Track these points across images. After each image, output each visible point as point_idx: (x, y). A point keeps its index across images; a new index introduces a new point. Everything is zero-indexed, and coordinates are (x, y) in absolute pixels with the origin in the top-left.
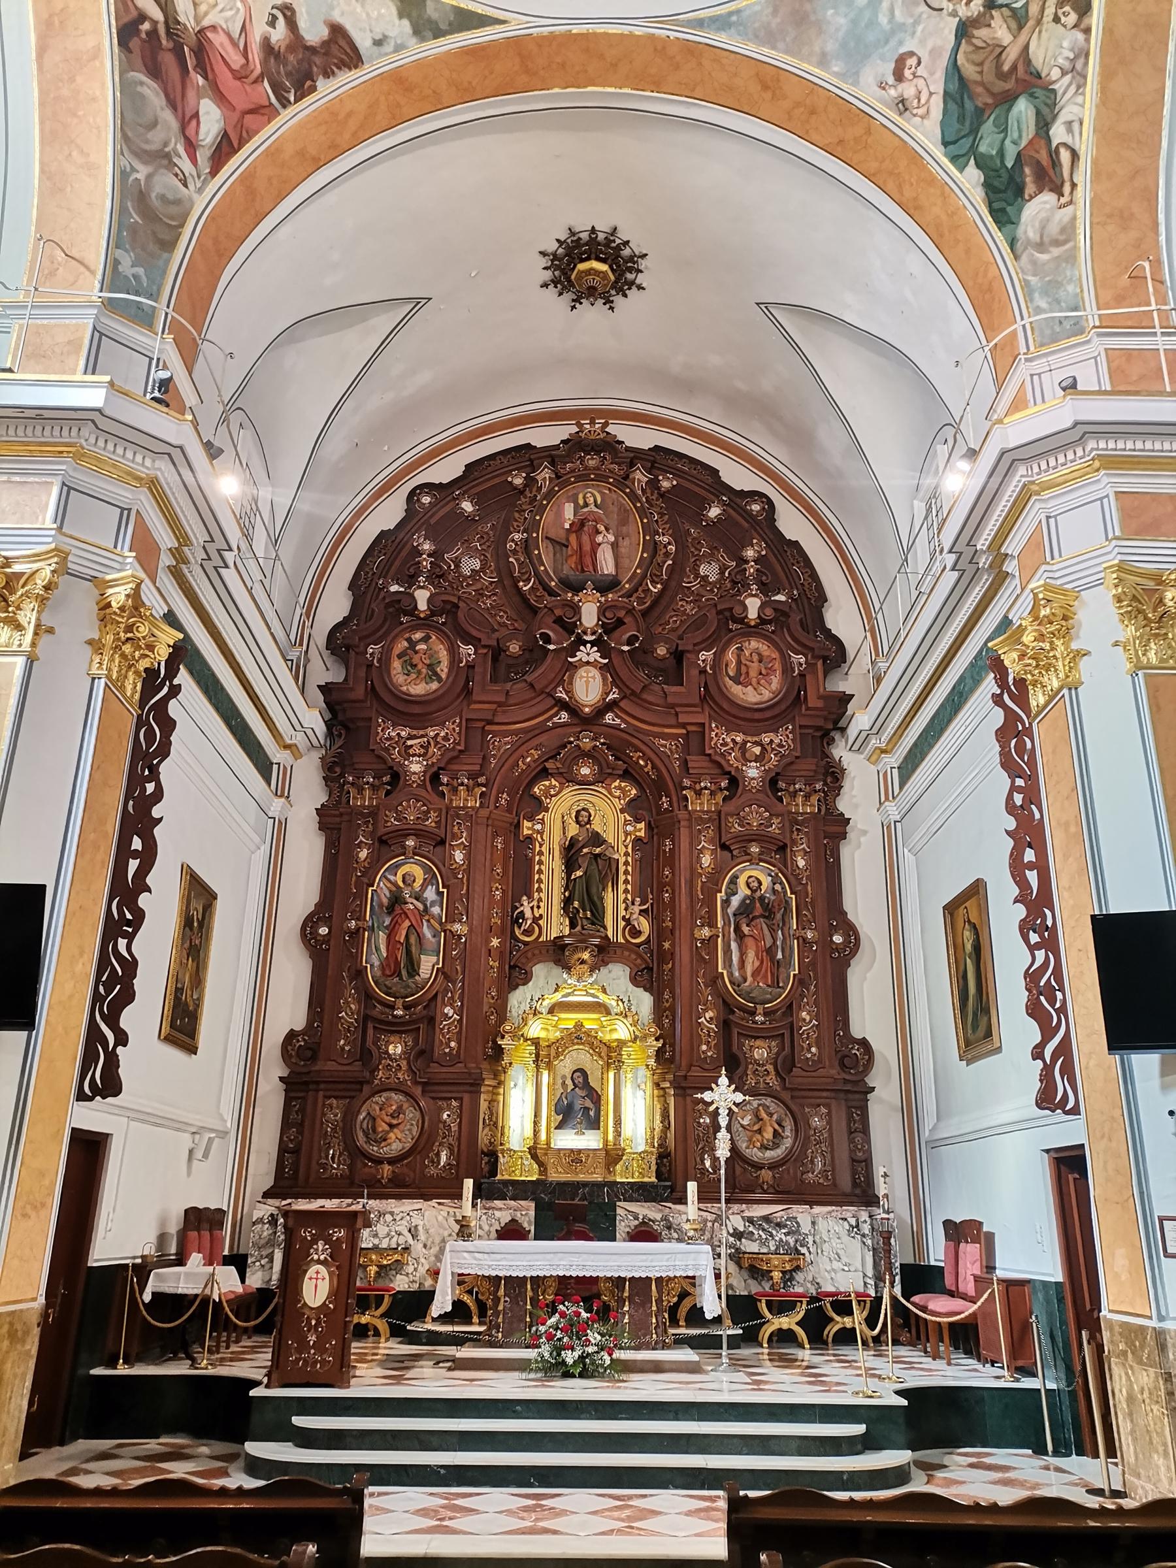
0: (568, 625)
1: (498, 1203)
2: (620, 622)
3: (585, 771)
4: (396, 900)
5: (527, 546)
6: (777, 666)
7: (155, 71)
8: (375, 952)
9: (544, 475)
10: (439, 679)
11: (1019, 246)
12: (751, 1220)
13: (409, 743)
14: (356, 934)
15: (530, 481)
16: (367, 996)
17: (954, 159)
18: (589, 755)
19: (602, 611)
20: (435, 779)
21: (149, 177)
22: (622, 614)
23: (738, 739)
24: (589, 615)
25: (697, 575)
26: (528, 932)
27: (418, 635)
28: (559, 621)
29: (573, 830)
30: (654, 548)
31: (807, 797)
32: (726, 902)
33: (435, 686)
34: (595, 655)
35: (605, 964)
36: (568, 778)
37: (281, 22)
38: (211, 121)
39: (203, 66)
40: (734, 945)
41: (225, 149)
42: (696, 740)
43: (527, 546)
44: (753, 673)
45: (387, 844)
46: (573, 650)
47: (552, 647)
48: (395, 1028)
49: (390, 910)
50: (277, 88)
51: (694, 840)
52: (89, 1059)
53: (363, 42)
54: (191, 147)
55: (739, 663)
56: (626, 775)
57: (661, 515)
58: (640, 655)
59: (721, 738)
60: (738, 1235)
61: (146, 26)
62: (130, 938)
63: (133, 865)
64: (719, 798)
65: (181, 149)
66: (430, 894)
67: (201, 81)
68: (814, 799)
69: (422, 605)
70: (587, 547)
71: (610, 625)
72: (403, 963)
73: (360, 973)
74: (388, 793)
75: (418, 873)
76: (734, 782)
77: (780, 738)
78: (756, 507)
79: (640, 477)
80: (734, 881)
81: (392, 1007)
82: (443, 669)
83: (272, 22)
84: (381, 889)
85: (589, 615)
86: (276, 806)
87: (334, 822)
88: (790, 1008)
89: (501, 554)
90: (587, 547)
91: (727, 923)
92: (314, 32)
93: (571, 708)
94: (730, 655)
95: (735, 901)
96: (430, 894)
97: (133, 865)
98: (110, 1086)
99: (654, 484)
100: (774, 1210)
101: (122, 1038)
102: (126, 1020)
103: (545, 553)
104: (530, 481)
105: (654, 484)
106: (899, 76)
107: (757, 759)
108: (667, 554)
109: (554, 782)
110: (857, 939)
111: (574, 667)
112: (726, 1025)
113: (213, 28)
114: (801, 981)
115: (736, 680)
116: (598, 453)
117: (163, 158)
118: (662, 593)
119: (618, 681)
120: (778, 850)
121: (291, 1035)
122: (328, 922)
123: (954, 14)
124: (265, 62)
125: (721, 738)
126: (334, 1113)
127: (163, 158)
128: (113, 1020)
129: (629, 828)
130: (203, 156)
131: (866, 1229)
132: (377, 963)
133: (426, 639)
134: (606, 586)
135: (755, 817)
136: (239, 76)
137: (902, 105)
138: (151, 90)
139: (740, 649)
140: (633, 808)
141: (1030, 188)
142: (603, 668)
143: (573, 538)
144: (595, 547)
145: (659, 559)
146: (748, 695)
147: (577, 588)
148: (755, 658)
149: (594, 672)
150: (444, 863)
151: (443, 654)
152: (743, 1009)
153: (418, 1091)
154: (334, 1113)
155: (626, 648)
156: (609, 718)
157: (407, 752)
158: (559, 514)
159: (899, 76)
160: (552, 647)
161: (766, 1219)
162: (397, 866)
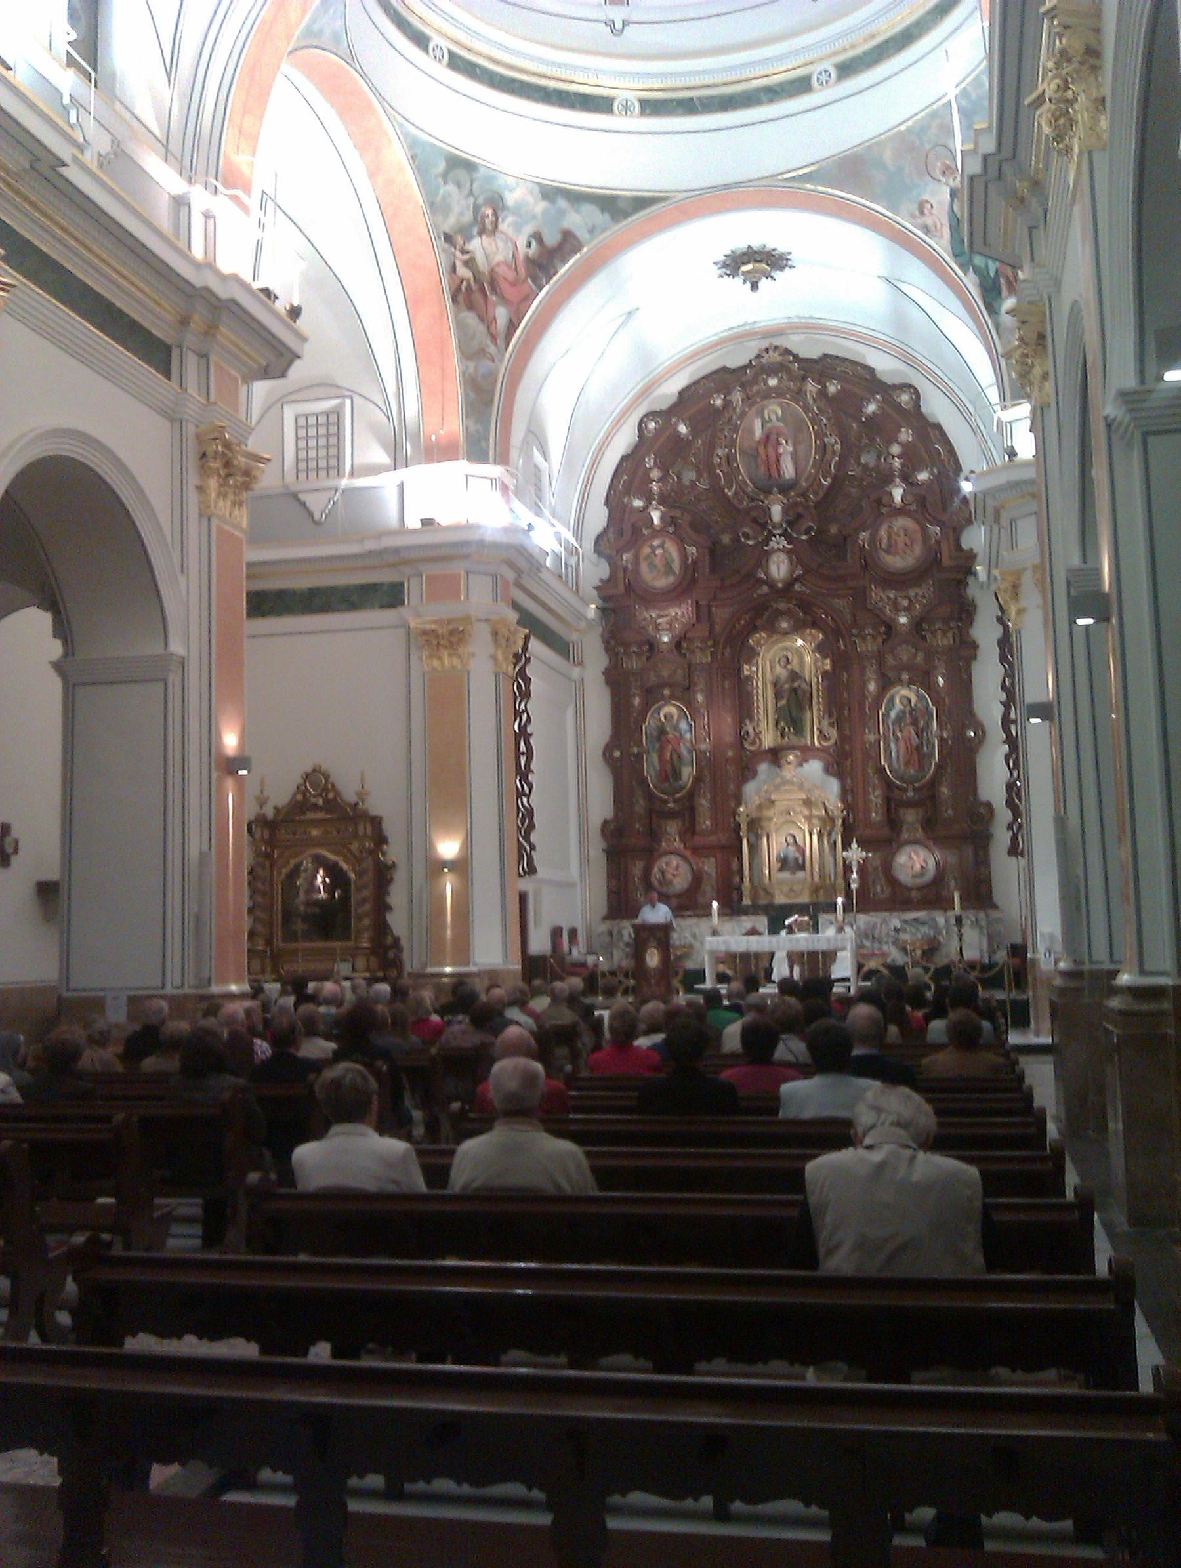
0: (761, 522)
1: (744, 918)
2: (799, 516)
3: (784, 625)
4: (662, 731)
5: (729, 459)
6: (919, 536)
7: (471, 307)
8: (651, 767)
9: (737, 397)
10: (675, 574)
11: (1000, 330)
12: (906, 922)
13: (659, 621)
14: (639, 757)
15: (727, 404)
16: (649, 796)
17: (961, 266)
18: (788, 613)
19: (785, 511)
20: (678, 645)
21: (476, 367)
22: (800, 510)
23: (892, 596)
24: (776, 512)
25: (859, 464)
26: (753, 743)
27: (656, 543)
28: (755, 521)
29: (779, 670)
30: (823, 449)
31: (945, 632)
32: (886, 716)
33: (671, 579)
34: (783, 542)
35: (807, 761)
36: (771, 629)
37: (534, 243)
38: (501, 314)
39: (494, 288)
40: (893, 745)
41: (512, 327)
42: (860, 597)
43: (729, 459)
44: (901, 545)
45: (652, 696)
46: (767, 541)
47: (751, 543)
48: (672, 815)
49: (659, 739)
50: (534, 280)
51: (863, 670)
52: (521, 858)
53: (582, 234)
54: (494, 338)
55: (889, 537)
56: (814, 624)
57: (828, 419)
58: (818, 540)
59: (878, 595)
60: (896, 930)
61: (465, 283)
62: (528, 797)
63: (523, 760)
64: (880, 640)
65: (489, 342)
66: (683, 726)
67: (494, 298)
68: (950, 635)
69: (656, 521)
70: (773, 458)
71: (793, 519)
72: (671, 773)
73: (643, 781)
74: (648, 659)
75: (674, 711)
76: (890, 627)
77: (922, 593)
78: (905, 398)
79: (811, 387)
80: (892, 699)
81: (666, 802)
82: (676, 566)
83: (529, 245)
84: (650, 724)
85: (776, 512)
86: (576, 672)
87: (616, 679)
88: (933, 784)
89: (711, 468)
90: (773, 458)
91: (886, 728)
92: (551, 240)
93: (770, 583)
94: (883, 533)
95: (893, 714)
96: (683, 726)
97: (523, 760)
98: (532, 870)
99: (823, 393)
100: (921, 914)
101: (533, 847)
102: (533, 837)
103: (740, 463)
104: (727, 404)
105: (823, 393)
106: (922, 212)
107: (907, 609)
108: (834, 453)
109: (763, 635)
110: (984, 732)
111: (767, 554)
112: (888, 800)
113: (498, 264)
114: (939, 766)
115: (888, 552)
116: (776, 375)
117: (482, 352)
118: (831, 486)
119: (800, 561)
120: (923, 679)
121: (605, 823)
122: (618, 747)
123: (947, 184)
124: (527, 269)
125: (878, 595)
126: (637, 869)
127: (482, 352)
128: (527, 838)
129: (819, 664)
130: (501, 342)
131: (983, 923)
132: (653, 774)
133: (662, 546)
134: (785, 488)
135: (905, 653)
136: (513, 284)
137: (927, 230)
138: (471, 318)
139: (890, 527)
140: (820, 649)
141: (1004, 292)
142: (789, 552)
143: (761, 450)
144: (778, 458)
145: (828, 456)
146: (897, 562)
147: (768, 492)
148: (902, 534)
149: (783, 557)
150: (690, 703)
151: (675, 554)
152: (898, 788)
153: (688, 853)
154: (637, 869)
155: (804, 537)
156: (797, 587)
157: (657, 627)
158: (751, 431)
159: (922, 212)
160: (751, 543)
161: (916, 920)
162: (660, 708)
